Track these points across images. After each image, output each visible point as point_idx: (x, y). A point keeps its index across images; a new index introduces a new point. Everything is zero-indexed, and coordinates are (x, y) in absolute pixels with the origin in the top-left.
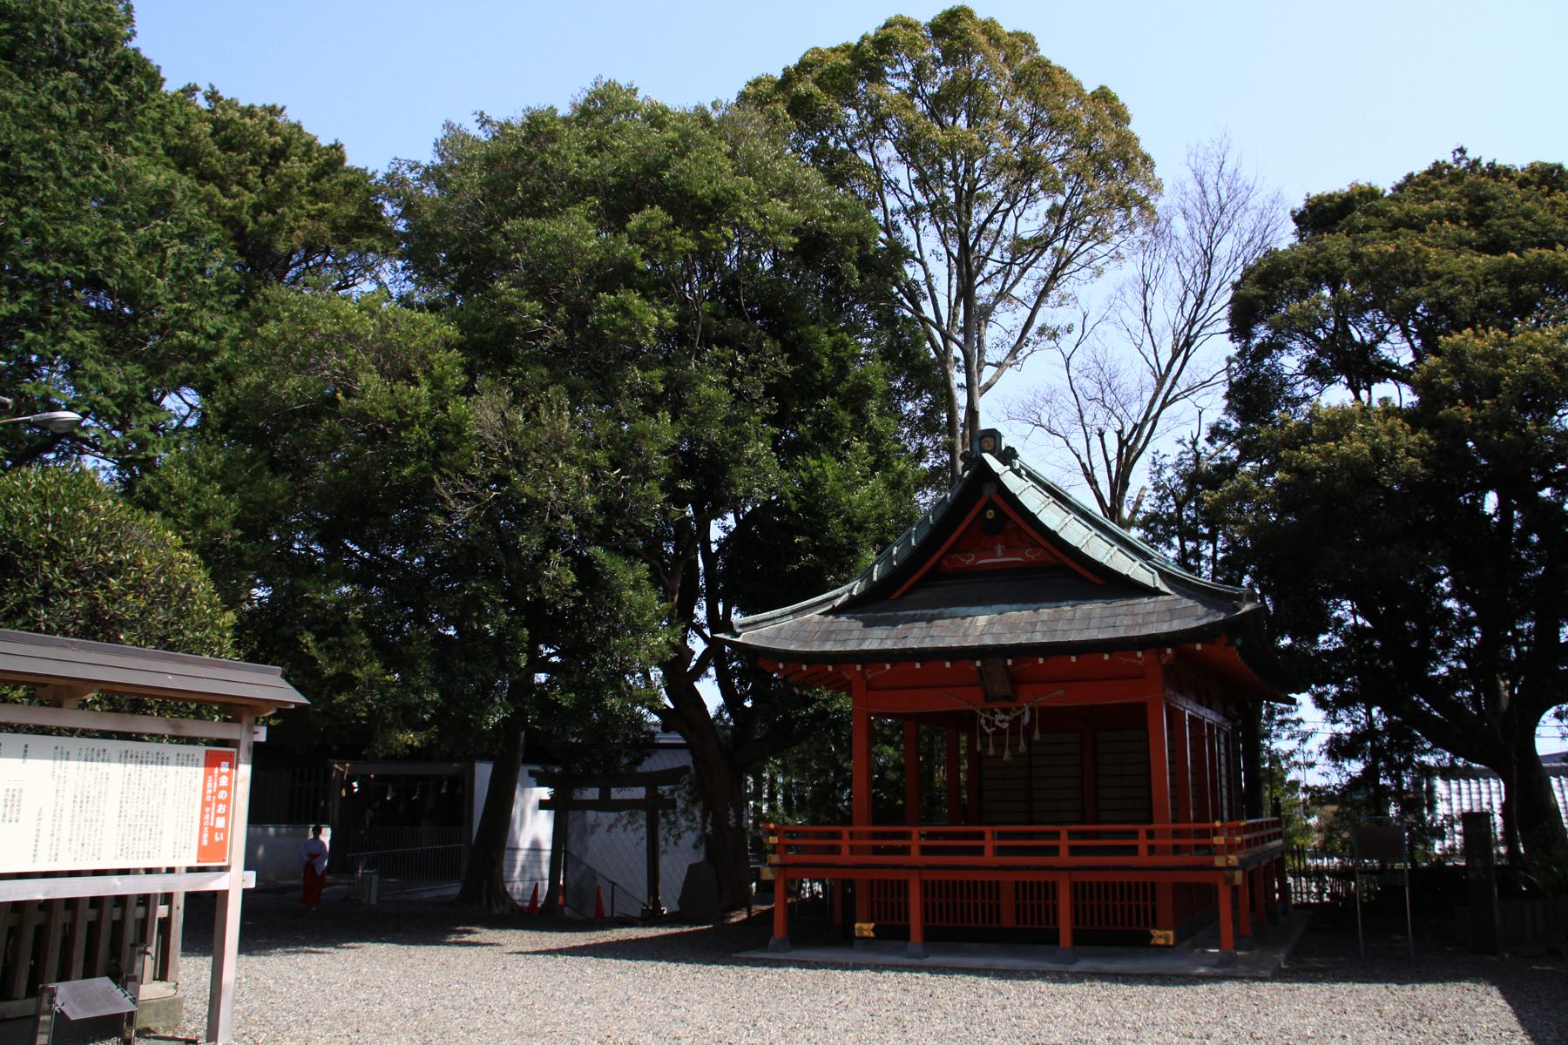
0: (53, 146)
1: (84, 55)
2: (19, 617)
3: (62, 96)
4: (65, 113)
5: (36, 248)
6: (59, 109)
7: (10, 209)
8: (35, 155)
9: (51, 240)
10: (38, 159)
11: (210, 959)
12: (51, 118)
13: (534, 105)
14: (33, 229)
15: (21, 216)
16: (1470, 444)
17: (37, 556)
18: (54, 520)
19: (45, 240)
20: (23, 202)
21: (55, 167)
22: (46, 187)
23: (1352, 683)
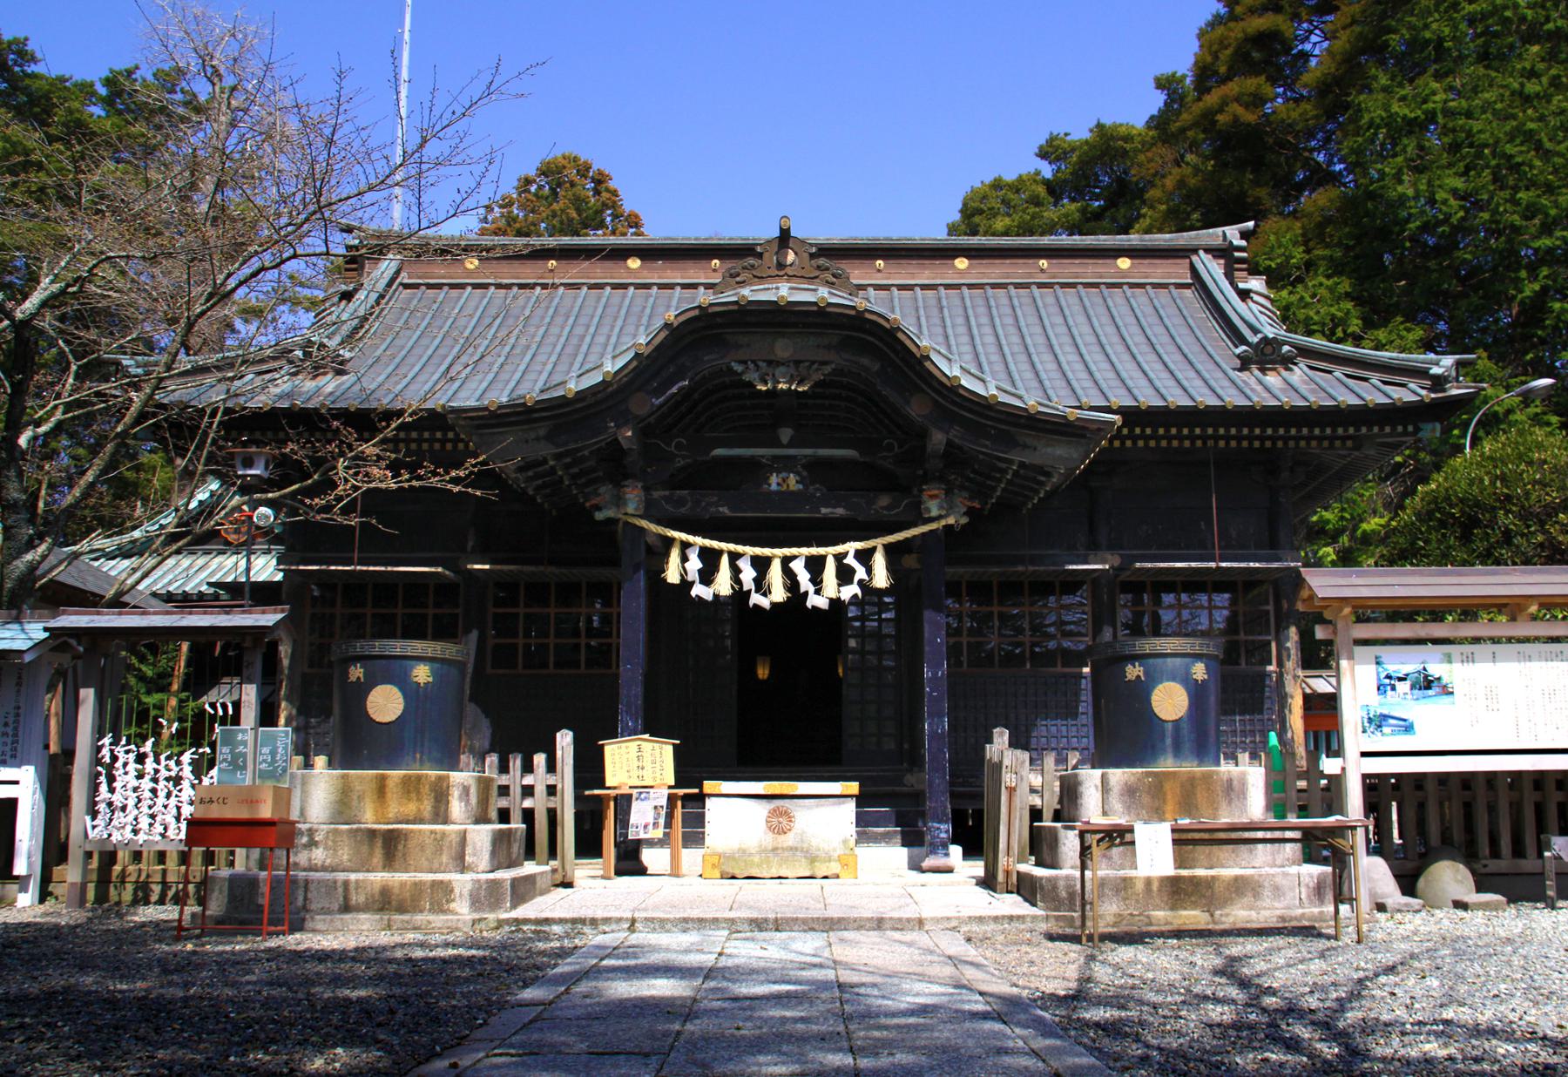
0: (1531, 126)
1: (1548, 20)
2: (3, 763)
3: (1532, 74)
4: (1538, 88)
5: (1543, 224)
6: (1532, 87)
7: (1507, 201)
8: (1518, 141)
9: (1553, 212)
10: (1522, 144)
11: (982, 863)
12: (1527, 99)
13: (1107, 121)
14: (1530, 212)
15: (1517, 203)
16: (763, 672)
17: (1494, 508)
18: (1503, 478)
19: (1547, 215)
20: (1516, 189)
21: (1539, 147)
22: (1532, 167)
23: (206, 1050)
